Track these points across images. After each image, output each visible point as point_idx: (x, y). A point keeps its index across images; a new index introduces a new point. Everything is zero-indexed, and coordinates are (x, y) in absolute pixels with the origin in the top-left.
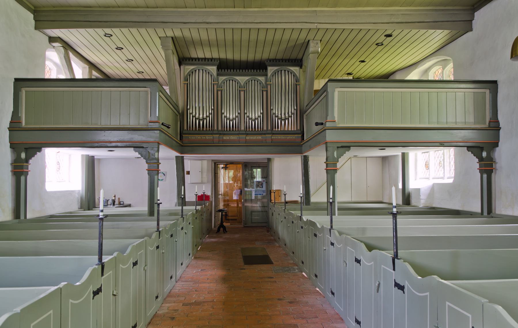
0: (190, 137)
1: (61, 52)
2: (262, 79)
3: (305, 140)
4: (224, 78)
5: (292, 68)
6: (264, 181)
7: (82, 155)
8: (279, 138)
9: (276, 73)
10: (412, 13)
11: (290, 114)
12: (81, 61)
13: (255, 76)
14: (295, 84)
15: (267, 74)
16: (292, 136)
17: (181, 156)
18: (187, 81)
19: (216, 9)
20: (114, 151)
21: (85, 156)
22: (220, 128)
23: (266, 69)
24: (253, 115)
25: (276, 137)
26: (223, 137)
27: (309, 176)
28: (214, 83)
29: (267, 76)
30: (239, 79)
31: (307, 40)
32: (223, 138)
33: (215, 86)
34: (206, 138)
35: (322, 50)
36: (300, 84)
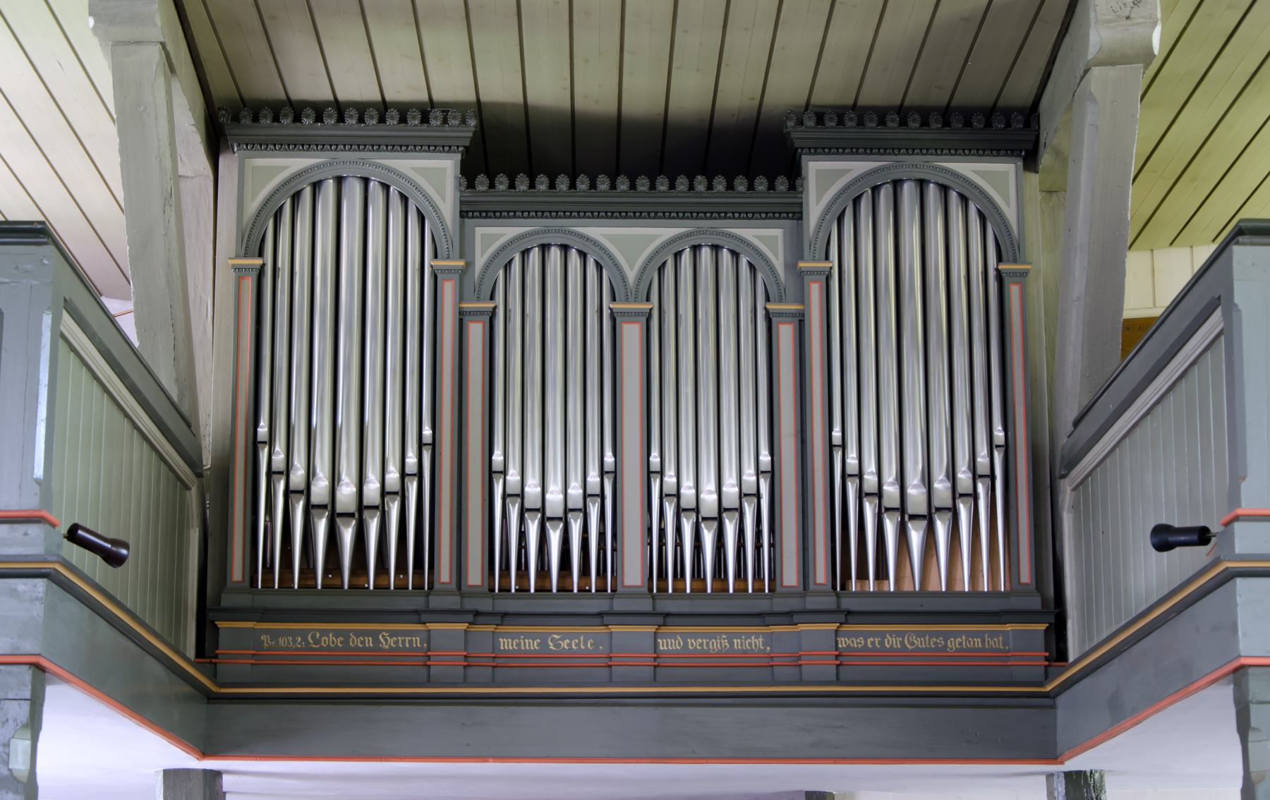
4: (507, 232)
8: (891, 642)
11: (963, 476)
15: (801, 204)
18: (261, 254)
22: (475, 576)
23: (794, 174)
24: (709, 485)
25: (866, 635)
29: (801, 218)
30: (609, 237)
34: (376, 641)
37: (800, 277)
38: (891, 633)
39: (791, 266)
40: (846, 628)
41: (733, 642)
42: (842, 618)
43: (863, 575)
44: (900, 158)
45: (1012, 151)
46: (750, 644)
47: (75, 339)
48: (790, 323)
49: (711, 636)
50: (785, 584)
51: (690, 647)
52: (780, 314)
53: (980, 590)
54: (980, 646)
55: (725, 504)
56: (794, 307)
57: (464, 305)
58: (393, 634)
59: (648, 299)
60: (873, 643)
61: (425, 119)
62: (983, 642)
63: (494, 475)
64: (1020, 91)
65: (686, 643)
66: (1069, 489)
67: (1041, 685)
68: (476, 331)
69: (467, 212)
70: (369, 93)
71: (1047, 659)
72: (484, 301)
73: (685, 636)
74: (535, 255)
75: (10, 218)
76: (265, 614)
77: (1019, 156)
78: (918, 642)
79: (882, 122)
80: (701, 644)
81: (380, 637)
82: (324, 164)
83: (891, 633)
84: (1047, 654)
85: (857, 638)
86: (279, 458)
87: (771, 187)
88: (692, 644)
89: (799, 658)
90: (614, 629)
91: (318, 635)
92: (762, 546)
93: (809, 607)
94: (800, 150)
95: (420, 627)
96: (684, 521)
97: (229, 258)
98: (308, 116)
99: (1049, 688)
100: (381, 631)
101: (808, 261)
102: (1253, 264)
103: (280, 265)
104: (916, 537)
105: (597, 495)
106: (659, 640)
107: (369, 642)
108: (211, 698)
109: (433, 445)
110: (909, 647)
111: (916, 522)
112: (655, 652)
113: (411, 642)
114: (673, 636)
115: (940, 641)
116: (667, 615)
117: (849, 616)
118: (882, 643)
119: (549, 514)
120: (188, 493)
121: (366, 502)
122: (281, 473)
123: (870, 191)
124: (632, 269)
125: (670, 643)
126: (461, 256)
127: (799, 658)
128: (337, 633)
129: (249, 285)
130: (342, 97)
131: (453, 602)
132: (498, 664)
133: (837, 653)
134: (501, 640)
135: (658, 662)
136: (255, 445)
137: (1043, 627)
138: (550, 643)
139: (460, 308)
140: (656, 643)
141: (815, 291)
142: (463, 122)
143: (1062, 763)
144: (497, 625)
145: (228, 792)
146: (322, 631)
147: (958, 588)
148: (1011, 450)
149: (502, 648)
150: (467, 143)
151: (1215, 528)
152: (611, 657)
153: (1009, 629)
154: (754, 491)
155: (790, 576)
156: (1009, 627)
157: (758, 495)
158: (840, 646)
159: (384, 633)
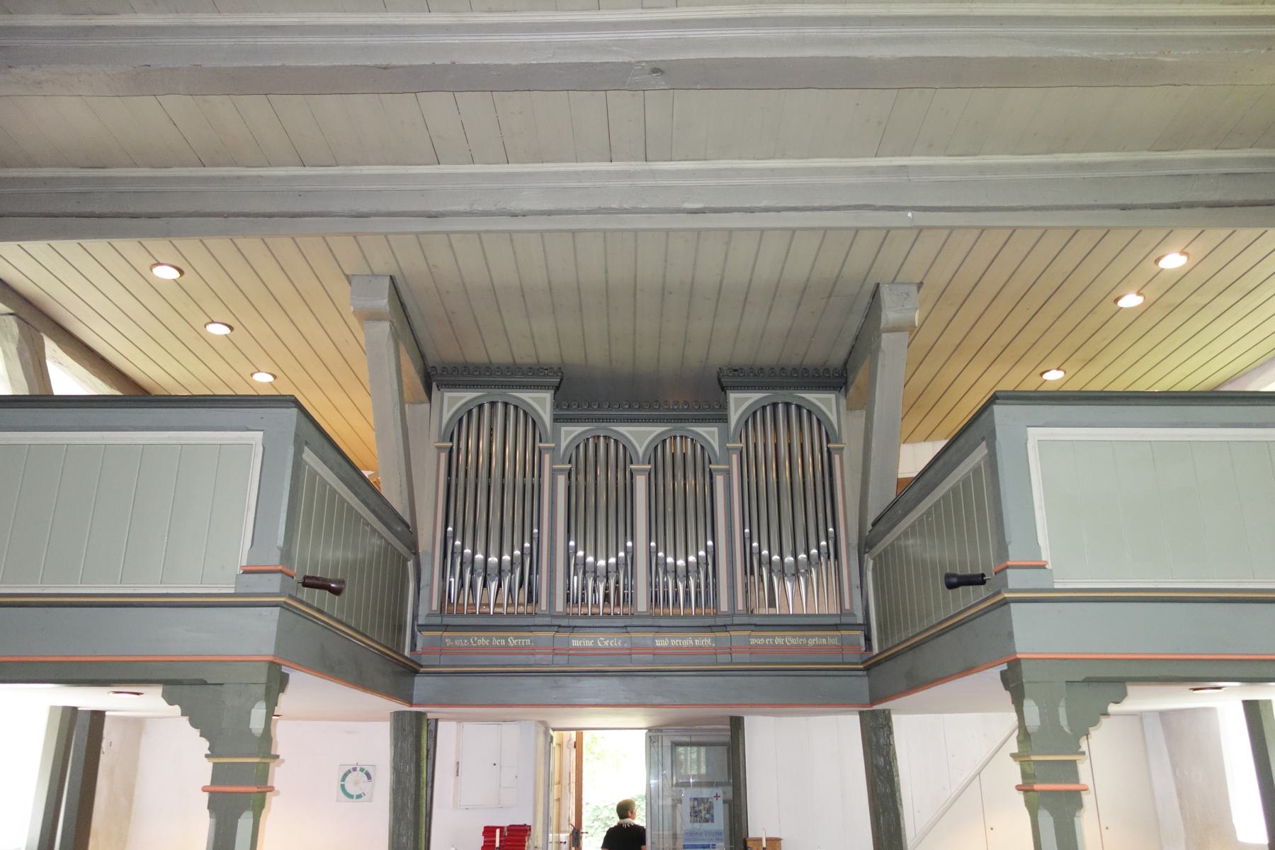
0: (447, 640)
1: (9, 336)
3: (877, 655)
4: (578, 429)
5: (813, 397)
6: (717, 797)
7: (53, 709)
8: (778, 641)
9: (751, 416)
10: (1260, 169)
12: (99, 377)
13: (687, 424)
14: (825, 449)
15: (726, 415)
16: (826, 637)
17: (417, 712)
18: (451, 440)
19: (545, 164)
20: (142, 694)
21: (60, 712)
25: (765, 637)
26: (654, 639)
27: (897, 794)
28: (541, 445)
29: (727, 422)
30: (630, 432)
31: (869, 287)
32: (569, 643)
33: (547, 458)
34: (507, 642)
35: (926, 315)
36: (842, 449)
46: (704, 643)
52: (717, 470)
65: (670, 643)
72: (566, 464)
73: (670, 639)
83: (778, 636)
113: (525, 642)
124: (641, 447)
129: (444, 456)
132: (570, 652)
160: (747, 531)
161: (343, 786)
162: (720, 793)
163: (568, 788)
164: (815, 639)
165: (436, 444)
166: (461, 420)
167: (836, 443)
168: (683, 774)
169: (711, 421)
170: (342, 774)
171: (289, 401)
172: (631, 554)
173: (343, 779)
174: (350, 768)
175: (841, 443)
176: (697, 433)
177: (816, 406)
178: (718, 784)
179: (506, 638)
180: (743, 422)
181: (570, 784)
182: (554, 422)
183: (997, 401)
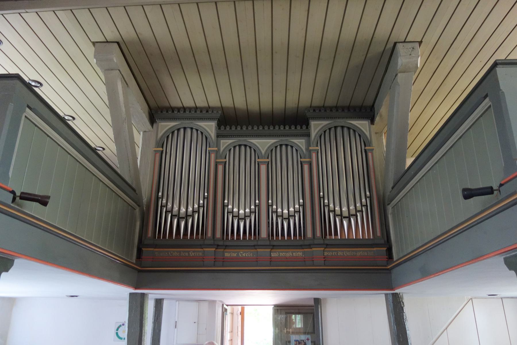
2: (300, 142)
3: (397, 261)
4: (229, 141)
6: (308, 339)
8: (340, 254)
15: (310, 133)
18: (162, 147)
22: (218, 235)
23: (308, 125)
25: (333, 251)
29: (310, 137)
30: (257, 142)
31: (390, 45)
32: (224, 254)
34: (189, 254)
36: (373, 150)
37: (310, 152)
38: (340, 251)
39: (307, 149)
40: (326, 249)
41: (293, 254)
42: (325, 246)
43: (330, 234)
44: (336, 120)
45: (367, 118)
46: (298, 254)
47: (45, 130)
48: (307, 164)
49: (286, 252)
50: (308, 237)
51: (281, 255)
52: (304, 162)
53: (365, 238)
54: (367, 255)
55: (290, 214)
56: (308, 160)
57: (217, 160)
58: (194, 252)
59: (268, 158)
60: (335, 254)
61: (207, 111)
62: (367, 253)
63: (225, 207)
64: (369, 102)
65: (279, 254)
66: (391, 208)
67: (386, 266)
68: (220, 168)
69: (219, 136)
70: (192, 105)
71: (387, 258)
72: (223, 159)
73: (279, 252)
74: (237, 148)
75: (11, 73)
76: (156, 246)
77: (369, 119)
78: (348, 254)
79: (331, 111)
80: (284, 255)
81: (190, 253)
82: (178, 124)
83: (340, 251)
84: (387, 257)
85: (330, 253)
86: (164, 201)
87: (301, 128)
88: (281, 255)
89: (313, 258)
90: (258, 250)
91: (172, 252)
92: (301, 227)
93: (316, 243)
94: (309, 119)
95: (202, 250)
96: (279, 219)
97: (153, 148)
98: (176, 111)
99: (389, 267)
100: (190, 251)
101: (312, 147)
102: (506, 74)
103: (167, 151)
104: (345, 223)
105: (254, 212)
106: (272, 253)
107: (187, 254)
108: (139, 271)
109: (207, 198)
110: (345, 255)
111: (345, 219)
112: (270, 257)
113: (199, 254)
114: (276, 252)
115: (355, 253)
116: (274, 246)
117: (327, 246)
118: (337, 254)
119: (240, 217)
120: (135, 211)
121: (188, 214)
122: (170, 212)
123: (328, 130)
124: (263, 150)
125: (275, 254)
126: (217, 147)
127: (313, 258)
128: (177, 252)
129: (158, 156)
130: (185, 105)
131: (211, 242)
132: (224, 261)
133: (324, 257)
134: (225, 253)
135: (271, 261)
136: (157, 198)
137: (385, 249)
138: (240, 254)
139: (216, 161)
140: (270, 254)
141: (314, 155)
142: (217, 112)
143: (394, 290)
144: (224, 249)
145: (165, 299)
146: (173, 251)
147: (358, 238)
148: (372, 198)
149: (226, 256)
150: (219, 118)
151: (495, 187)
152: (257, 258)
153: (375, 249)
154: (298, 211)
155: (309, 234)
156: (375, 249)
157: (300, 212)
158: (325, 255)
159: (192, 252)
160: (321, 194)
161: (117, 334)
162: (310, 338)
163: (237, 334)
164: (360, 252)
165: (154, 149)
166: (168, 137)
167: (370, 146)
168: (294, 327)
169: (301, 136)
170: (117, 327)
171: (16, 77)
172: (259, 206)
173: (117, 330)
174: (121, 324)
175: (373, 147)
176: (294, 143)
177: (358, 127)
178: (308, 333)
179: (189, 252)
180: (318, 136)
181: (238, 332)
182: (217, 137)
183: (498, 66)
